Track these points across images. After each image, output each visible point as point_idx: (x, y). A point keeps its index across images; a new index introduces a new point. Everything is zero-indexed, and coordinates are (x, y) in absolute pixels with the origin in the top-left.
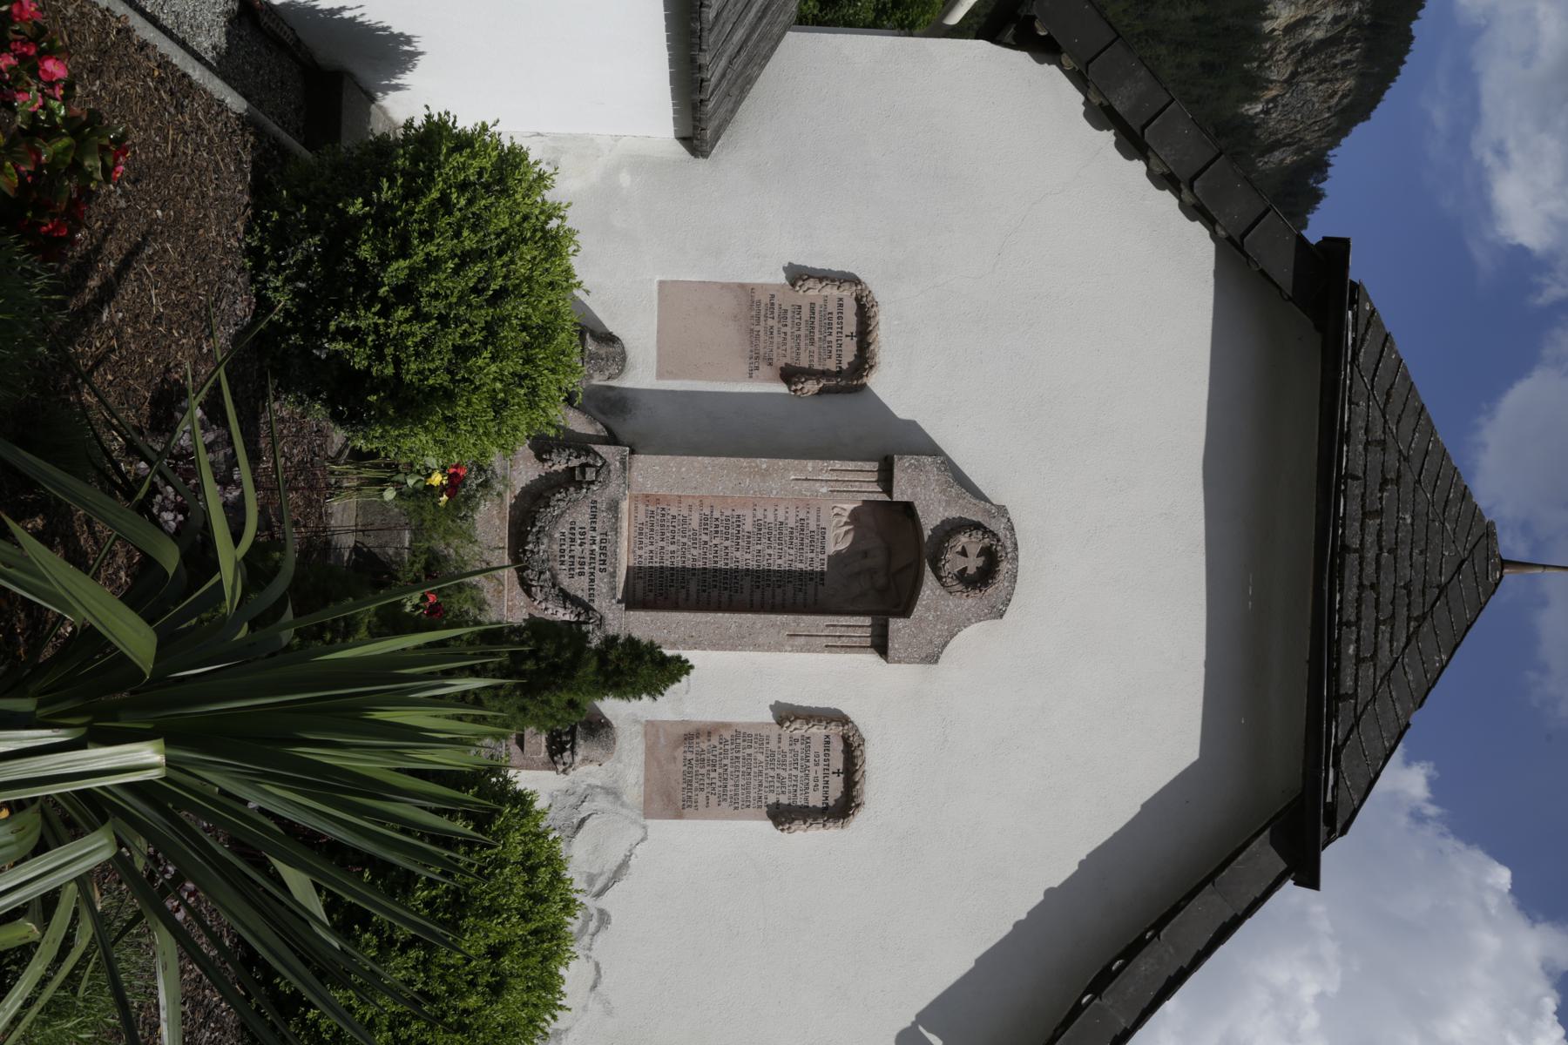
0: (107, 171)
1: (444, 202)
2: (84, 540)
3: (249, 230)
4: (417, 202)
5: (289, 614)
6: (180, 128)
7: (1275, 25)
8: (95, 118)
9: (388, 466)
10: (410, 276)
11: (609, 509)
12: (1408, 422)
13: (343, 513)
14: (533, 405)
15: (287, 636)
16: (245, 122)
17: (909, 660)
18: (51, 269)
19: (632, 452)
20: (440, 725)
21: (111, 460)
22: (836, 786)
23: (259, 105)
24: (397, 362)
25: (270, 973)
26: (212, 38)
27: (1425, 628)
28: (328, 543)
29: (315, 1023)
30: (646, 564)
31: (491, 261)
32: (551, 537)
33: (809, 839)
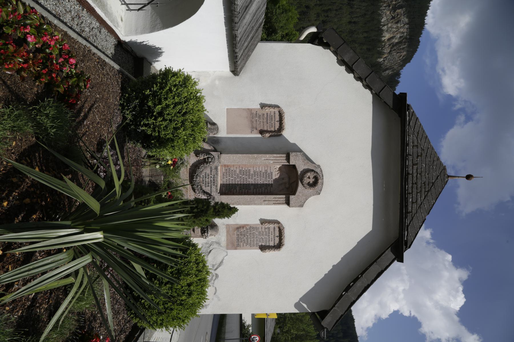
0: (85, 86)
1: (170, 90)
2: (81, 180)
3: (120, 99)
4: (163, 90)
5: (133, 199)
6: (103, 74)
7: (385, 38)
8: (82, 73)
9: (157, 159)
10: (162, 109)
11: (215, 169)
12: (423, 140)
13: (146, 172)
14: (194, 142)
15: (133, 204)
16: (119, 72)
17: (295, 206)
18: (72, 111)
19: (221, 154)
20: (173, 226)
21: (87, 160)
22: (277, 240)
23: (123, 67)
24: (159, 132)
25: (132, 291)
26: (111, 51)
27: (429, 194)
28: (142, 180)
29: (144, 303)
30: (225, 183)
31: (183, 105)
32: (200, 177)
33: (270, 254)
